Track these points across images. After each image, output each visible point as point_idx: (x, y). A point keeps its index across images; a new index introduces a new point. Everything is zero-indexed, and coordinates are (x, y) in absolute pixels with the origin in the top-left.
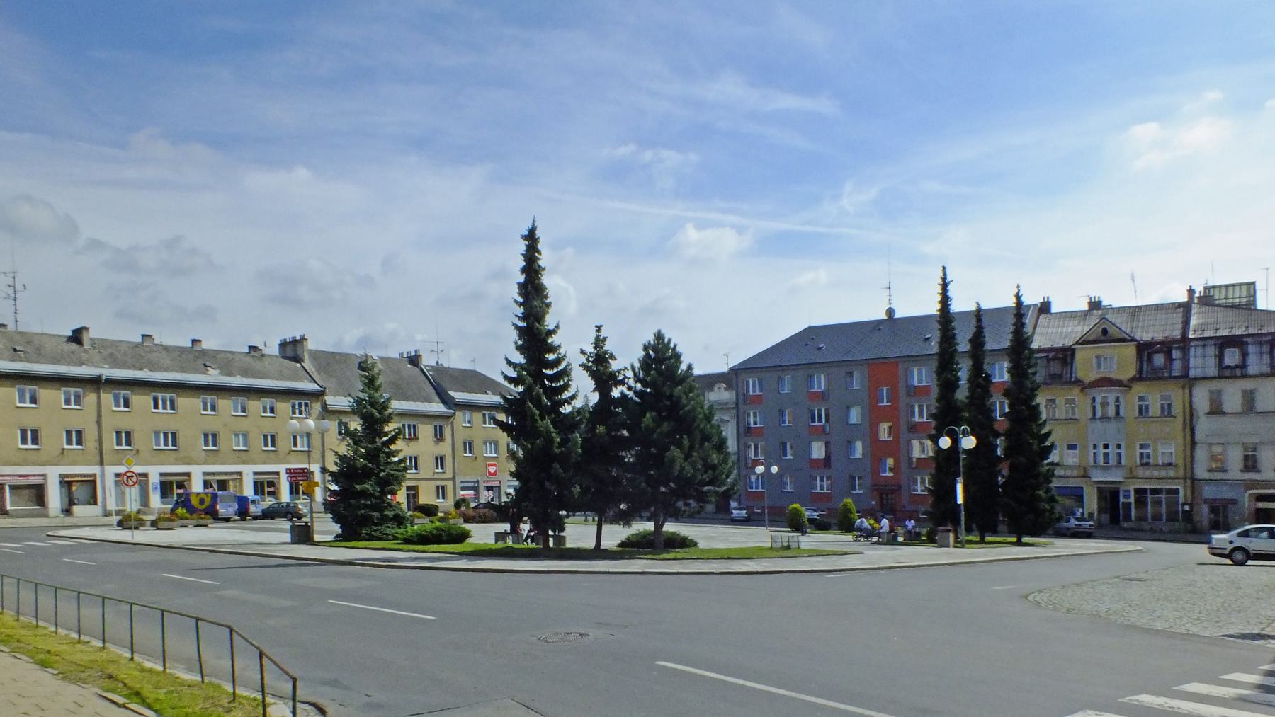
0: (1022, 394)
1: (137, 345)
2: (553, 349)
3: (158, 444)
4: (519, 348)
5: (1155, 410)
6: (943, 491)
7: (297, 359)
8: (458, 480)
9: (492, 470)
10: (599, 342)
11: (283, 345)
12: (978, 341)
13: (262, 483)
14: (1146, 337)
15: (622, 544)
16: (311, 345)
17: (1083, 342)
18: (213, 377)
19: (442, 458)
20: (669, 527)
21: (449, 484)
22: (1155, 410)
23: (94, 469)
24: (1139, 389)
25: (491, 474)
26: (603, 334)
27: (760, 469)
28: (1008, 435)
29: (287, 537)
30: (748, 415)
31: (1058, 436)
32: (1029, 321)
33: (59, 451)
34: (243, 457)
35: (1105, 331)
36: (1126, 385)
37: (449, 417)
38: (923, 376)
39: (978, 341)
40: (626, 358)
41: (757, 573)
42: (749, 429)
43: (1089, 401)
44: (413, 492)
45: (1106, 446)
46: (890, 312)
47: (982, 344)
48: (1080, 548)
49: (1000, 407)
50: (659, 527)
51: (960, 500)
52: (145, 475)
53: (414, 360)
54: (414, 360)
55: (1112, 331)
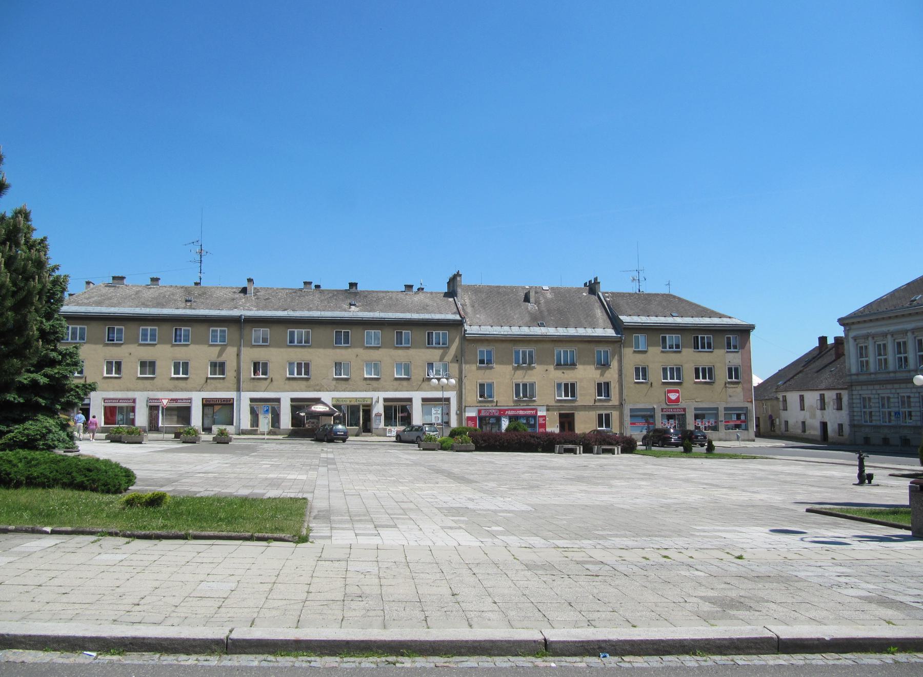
1: (301, 290)
3: (665, 378)
9: (673, 396)
16: (465, 281)
19: (573, 385)
21: (615, 415)
23: (231, 395)
25: (670, 400)
33: (203, 380)
34: (373, 383)
54: (592, 287)
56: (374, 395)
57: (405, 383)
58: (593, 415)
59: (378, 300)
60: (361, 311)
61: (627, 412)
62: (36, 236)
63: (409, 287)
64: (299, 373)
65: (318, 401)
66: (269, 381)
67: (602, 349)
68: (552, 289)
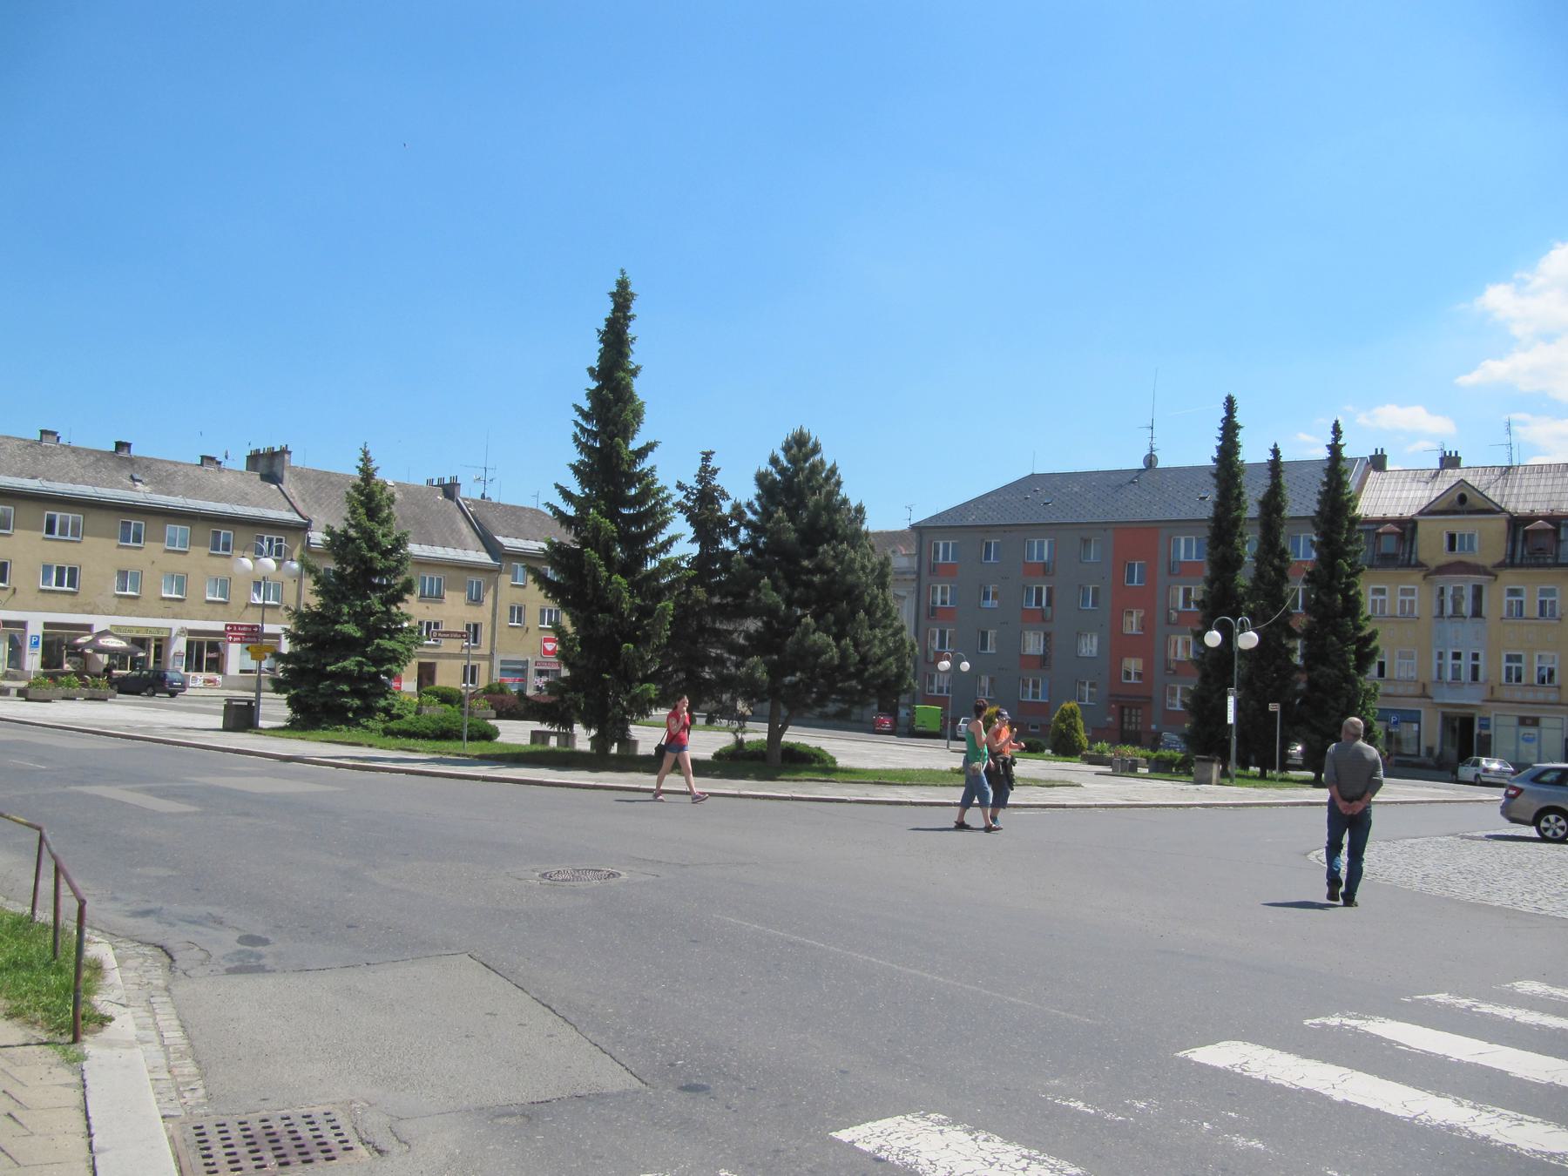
0: (1333, 580)
1: (33, 444)
2: (634, 478)
4: (576, 469)
5: (1531, 609)
6: (1206, 709)
7: (272, 477)
8: (498, 658)
10: (706, 474)
11: (254, 459)
12: (1272, 503)
13: (200, 645)
14: (1522, 507)
15: (717, 756)
16: (295, 460)
17: (1430, 511)
18: (142, 494)
19: (476, 626)
20: (795, 736)
21: (484, 665)
22: (1531, 609)
24: (1509, 578)
26: (713, 464)
27: (945, 665)
28: (1308, 635)
29: (218, 721)
30: (935, 589)
31: (1388, 644)
32: (1352, 480)
34: (173, 607)
35: (1462, 499)
36: (1491, 572)
37: (492, 571)
38: (1189, 549)
39: (1272, 503)
40: (739, 488)
41: (912, 804)
42: (934, 609)
43: (1436, 592)
44: (426, 673)
45: (1457, 656)
46: (1150, 460)
47: (1279, 509)
48: (1410, 793)
49: (1297, 589)
50: (775, 734)
51: (1231, 719)
52: (23, 624)
53: (450, 490)
54: (450, 490)
55: (1473, 499)
56: (176, 625)
57: (220, 608)
58: (459, 665)
59: (170, 476)
60: (156, 492)
61: (497, 666)
62: (853, 504)
63: (207, 460)
64: (60, 582)
65: (88, 628)
66: (10, 592)
67: (475, 578)
68: (397, 484)
